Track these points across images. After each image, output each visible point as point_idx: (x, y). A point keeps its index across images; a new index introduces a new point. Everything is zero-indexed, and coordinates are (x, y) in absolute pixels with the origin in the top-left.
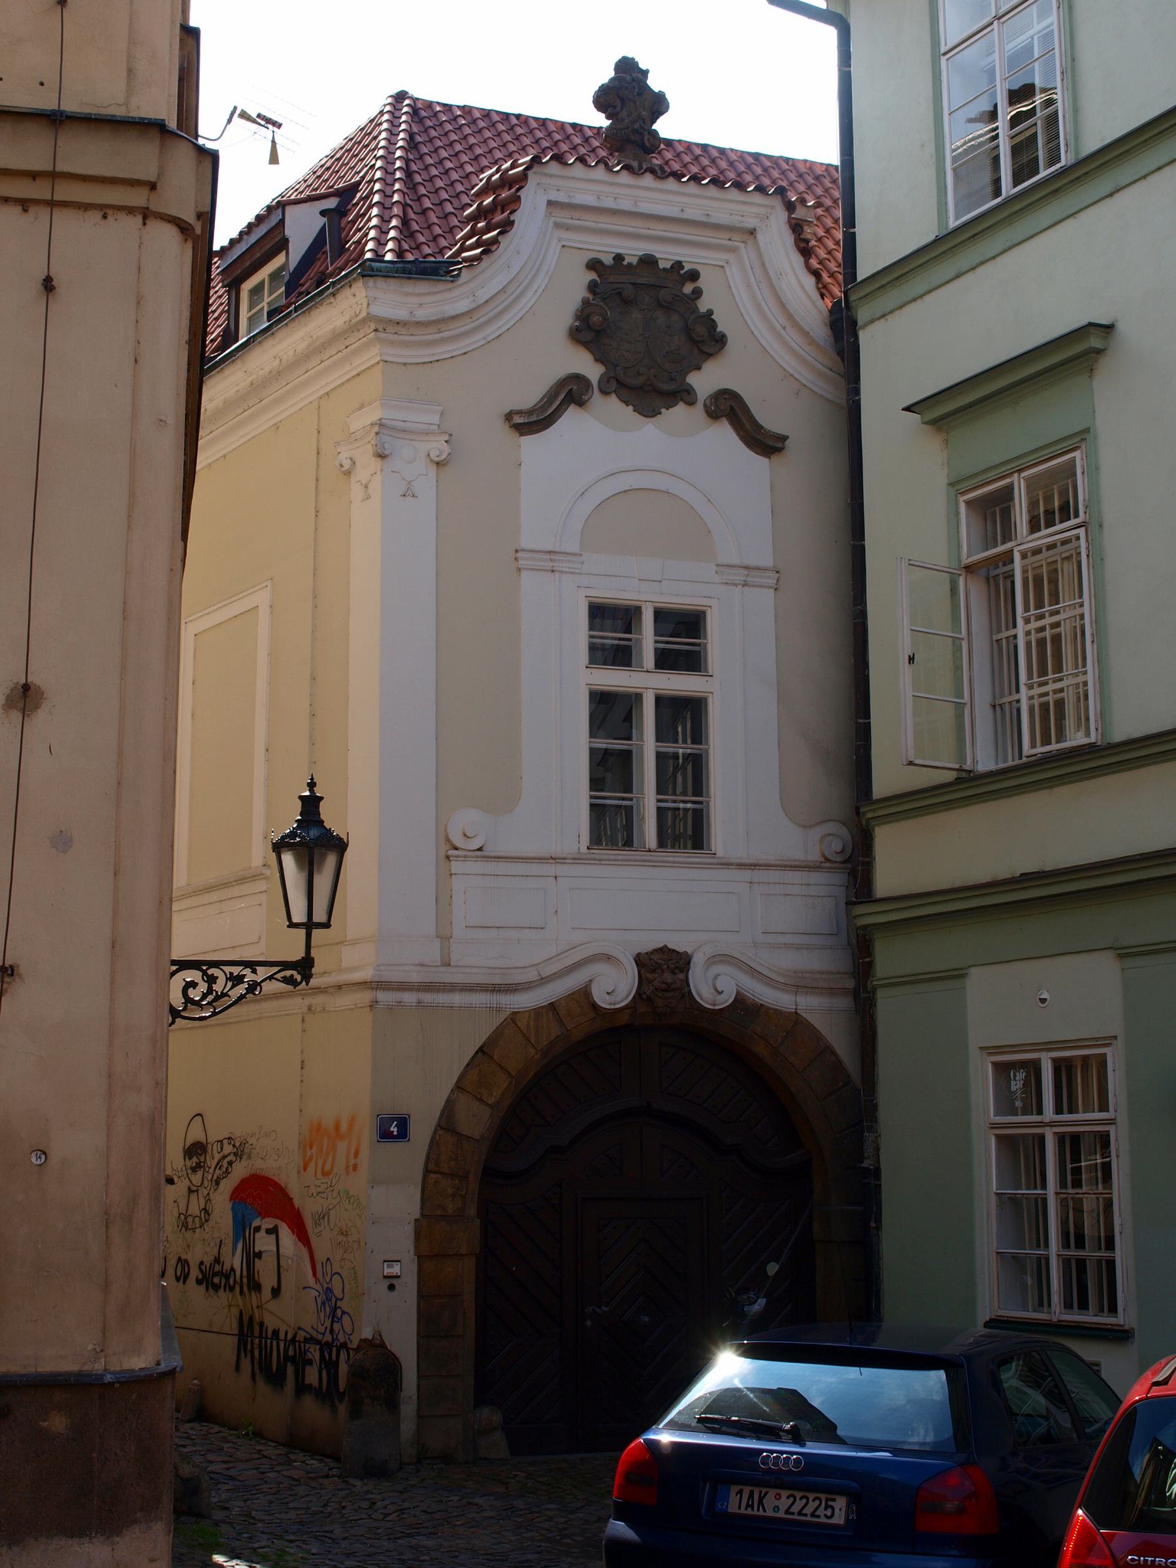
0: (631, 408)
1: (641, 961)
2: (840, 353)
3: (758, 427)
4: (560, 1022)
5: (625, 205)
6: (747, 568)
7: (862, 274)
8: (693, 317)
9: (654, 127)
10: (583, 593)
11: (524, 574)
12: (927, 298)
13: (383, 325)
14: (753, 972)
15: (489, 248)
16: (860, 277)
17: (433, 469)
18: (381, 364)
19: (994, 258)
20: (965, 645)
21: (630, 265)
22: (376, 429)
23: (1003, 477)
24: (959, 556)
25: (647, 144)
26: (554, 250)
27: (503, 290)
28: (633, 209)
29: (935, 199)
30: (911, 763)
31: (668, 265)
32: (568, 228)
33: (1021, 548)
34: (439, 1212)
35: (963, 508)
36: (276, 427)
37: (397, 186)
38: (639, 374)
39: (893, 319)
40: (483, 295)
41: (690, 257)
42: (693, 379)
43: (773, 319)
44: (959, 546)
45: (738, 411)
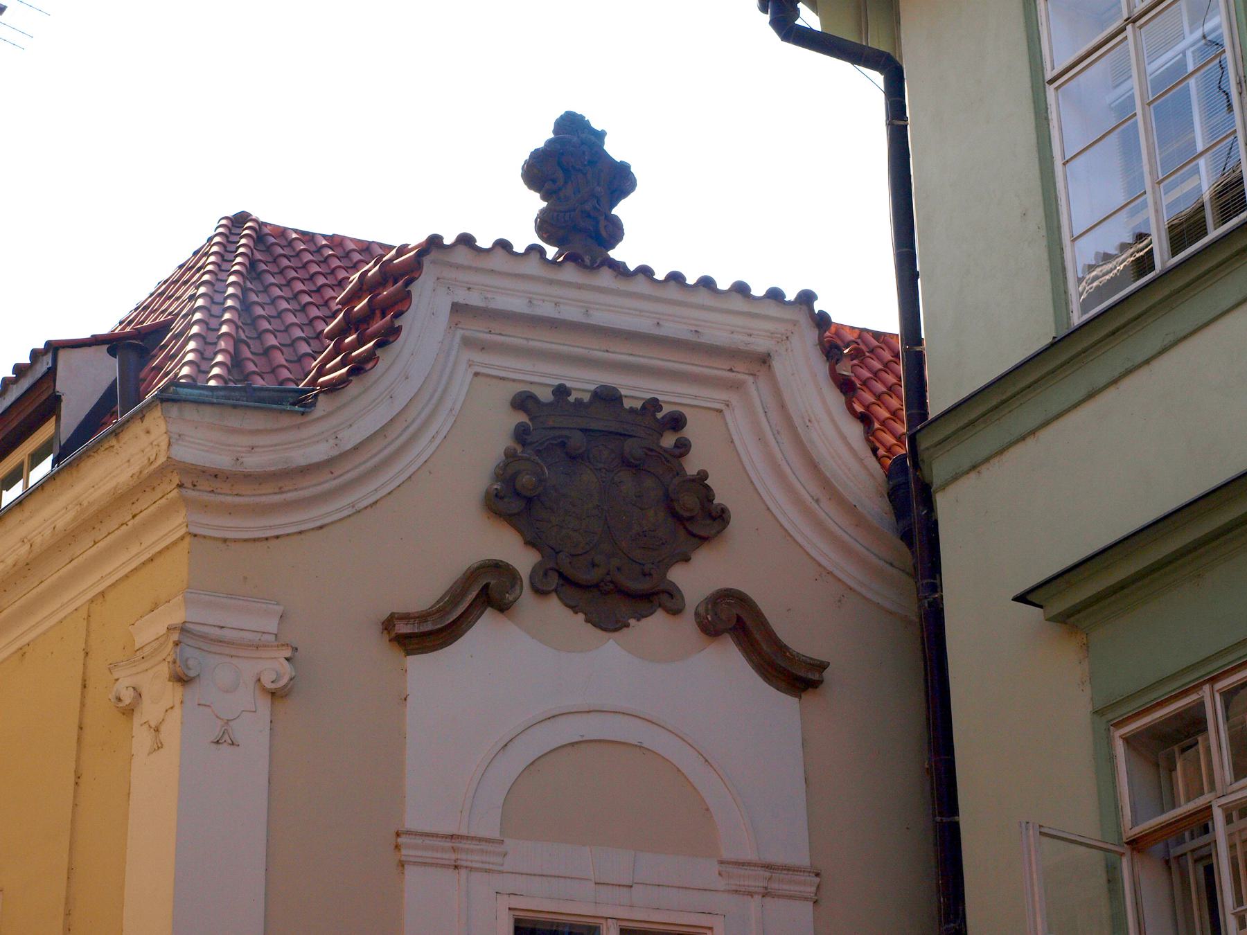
0: (581, 616)
2: (907, 537)
3: (782, 648)
5: (571, 313)
6: (768, 867)
7: (934, 410)
8: (676, 480)
9: (614, 211)
10: (505, 903)
11: (410, 871)
12: (1044, 434)
13: (195, 478)
15: (358, 369)
16: (933, 412)
17: (264, 705)
18: (187, 540)
19: (1147, 362)
21: (579, 402)
22: (175, 636)
23: (1185, 693)
24: (1118, 825)
25: (604, 233)
26: (463, 378)
27: (381, 432)
28: (584, 320)
29: (1048, 288)
31: (638, 405)
32: (483, 347)
33: (1223, 801)
35: (1120, 748)
36: (22, 653)
37: (227, 316)
38: (594, 565)
39: (991, 472)
40: (351, 438)
41: (672, 395)
42: (678, 575)
43: (798, 486)
44: (1117, 808)
45: (749, 623)
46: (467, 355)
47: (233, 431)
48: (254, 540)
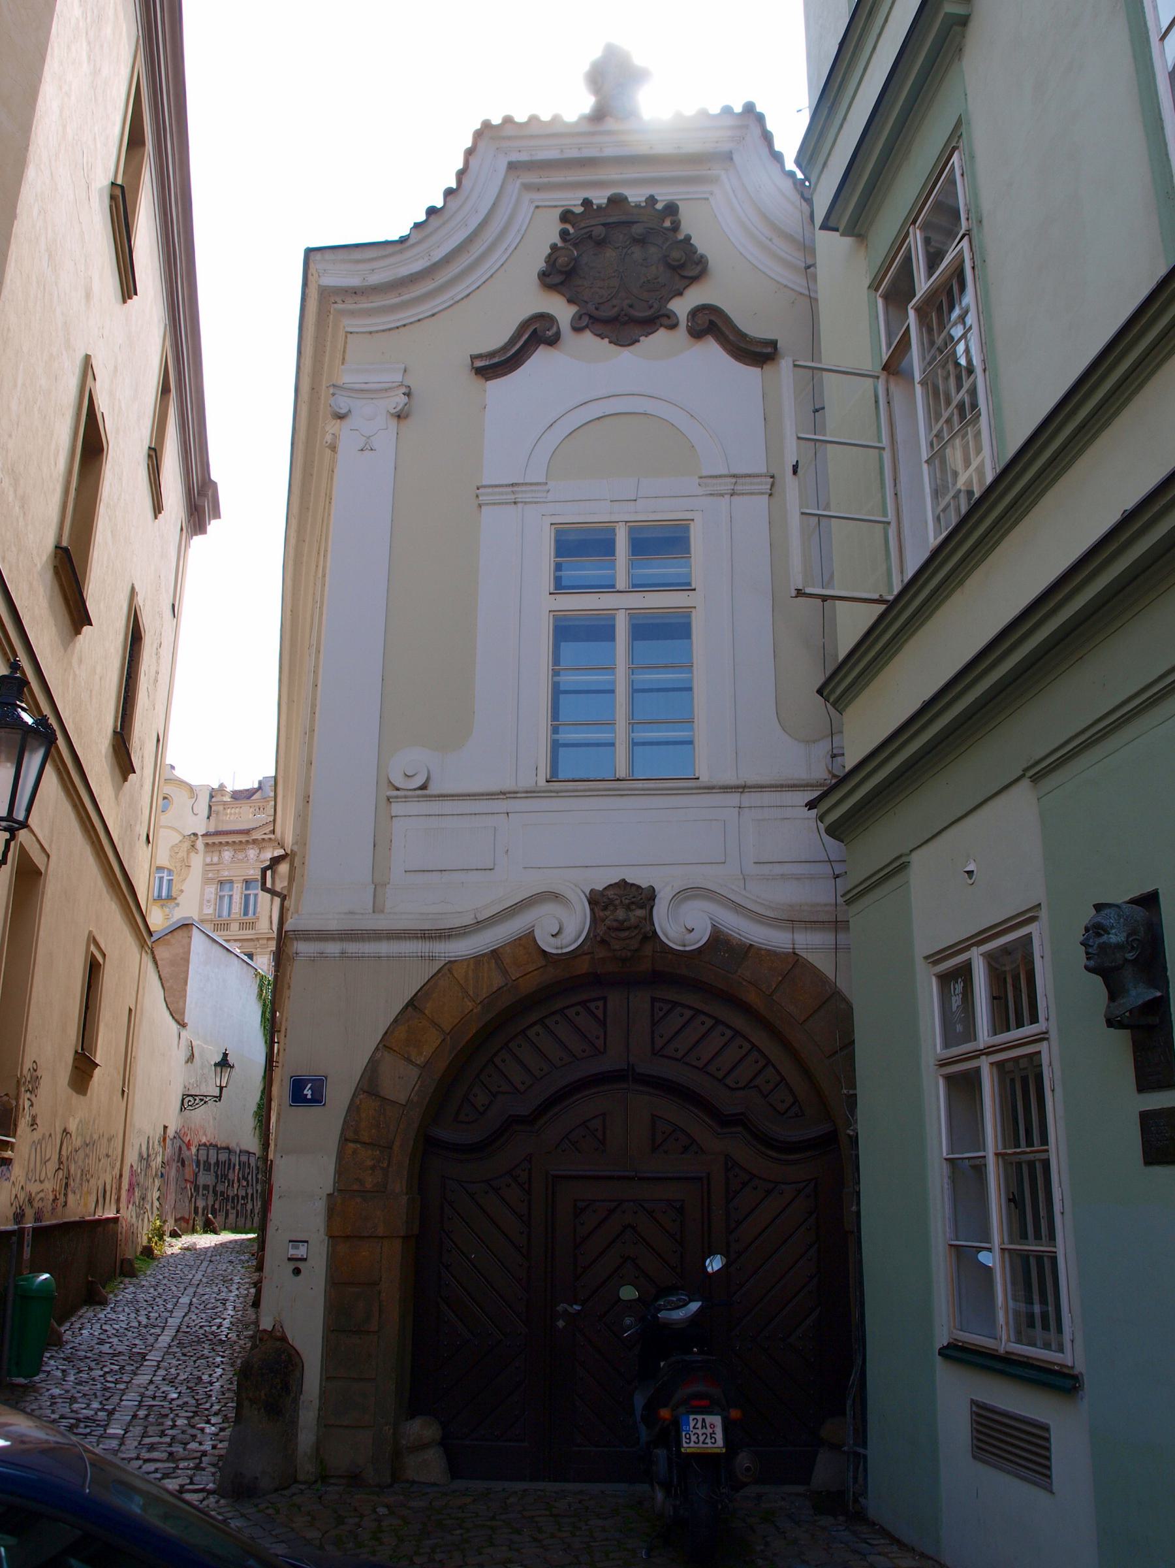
1: (597, 900)
3: (743, 336)
4: (505, 972)
6: (734, 476)
14: (737, 908)
17: (393, 423)
20: (887, 455)
21: (599, 207)
30: (800, 593)
32: (539, 188)
34: (355, 1187)
41: (664, 195)
46: (527, 196)
47: (358, 262)
48: (390, 329)
